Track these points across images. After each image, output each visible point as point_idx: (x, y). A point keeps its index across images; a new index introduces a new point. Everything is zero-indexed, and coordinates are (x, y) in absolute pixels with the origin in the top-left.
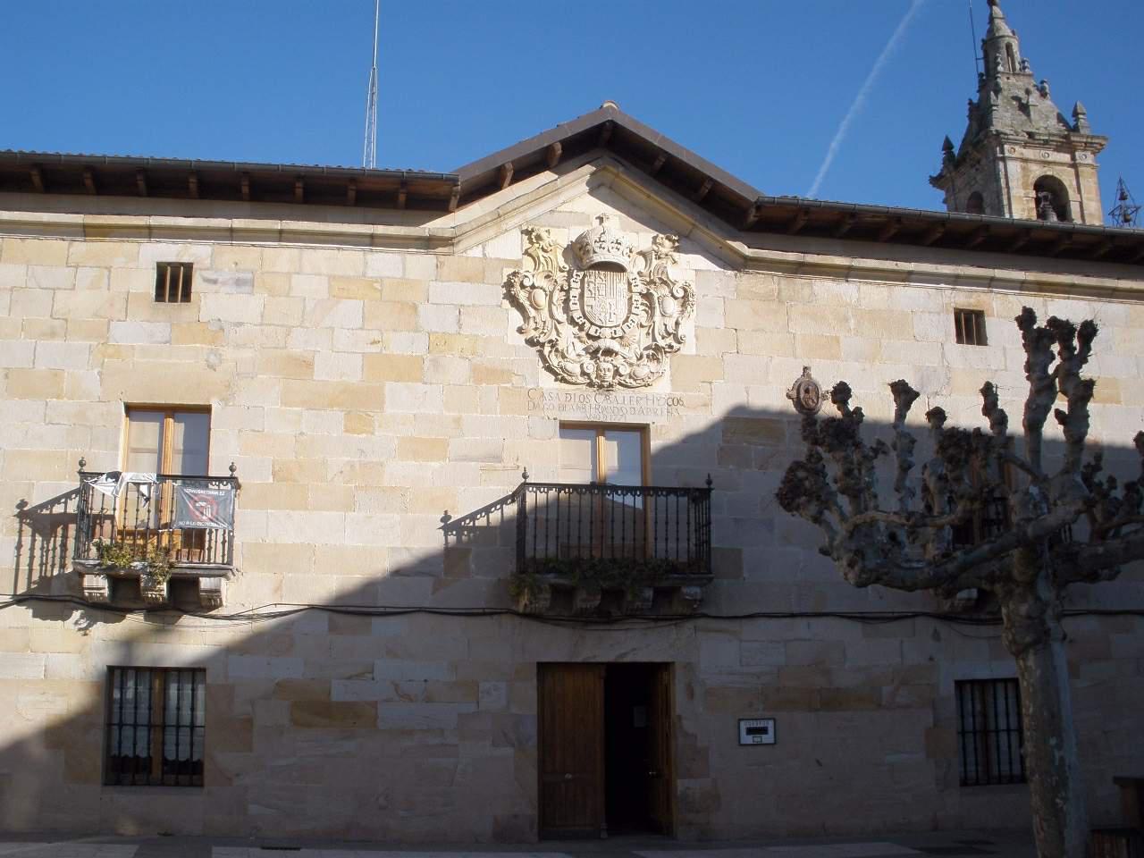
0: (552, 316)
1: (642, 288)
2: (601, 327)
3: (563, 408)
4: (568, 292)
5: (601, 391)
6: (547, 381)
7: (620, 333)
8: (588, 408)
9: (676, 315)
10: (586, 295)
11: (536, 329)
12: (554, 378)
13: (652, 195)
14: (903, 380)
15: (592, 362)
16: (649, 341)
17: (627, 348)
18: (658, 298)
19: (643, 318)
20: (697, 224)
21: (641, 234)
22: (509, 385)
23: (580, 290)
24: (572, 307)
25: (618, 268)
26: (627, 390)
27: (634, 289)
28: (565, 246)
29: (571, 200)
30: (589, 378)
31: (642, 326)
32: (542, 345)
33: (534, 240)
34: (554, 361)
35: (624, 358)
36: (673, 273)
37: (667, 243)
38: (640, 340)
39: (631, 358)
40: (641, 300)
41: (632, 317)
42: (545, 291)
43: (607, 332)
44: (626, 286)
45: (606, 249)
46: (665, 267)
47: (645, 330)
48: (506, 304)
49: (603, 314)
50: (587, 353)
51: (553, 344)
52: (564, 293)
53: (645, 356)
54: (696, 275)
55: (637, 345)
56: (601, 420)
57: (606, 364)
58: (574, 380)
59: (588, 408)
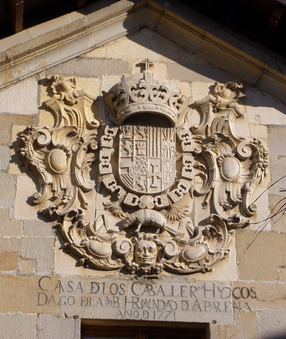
0: (75, 182)
1: (194, 146)
2: (140, 195)
3: (86, 302)
4: (97, 152)
5: (140, 279)
6: (66, 266)
7: (165, 202)
8: (121, 301)
9: (242, 180)
10: (120, 155)
11: (53, 199)
12: (75, 262)
13: (209, 35)
14: (80, 206)
15: (129, 240)
16: (206, 214)
17: (177, 223)
18: (218, 159)
19: (198, 185)
20: (266, 67)
21: (194, 84)
22: (13, 272)
23: (113, 150)
24: (102, 170)
25: (161, 121)
26: (176, 277)
27: (185, 148)
28: (95, 98)
29: (103, 44)
30: (124, 261)
31: (196, 194)
32: (61, 219)
33: (55, 91)
34: (76, 239)
35: (173, 235)
36: (236, 129)
37: (228, 93)
38: (195, 212)
39: (182, 235)
40: (194, 162)
41: (182, 182)
42: (66, 150)
43: (149, 201)
44: (174, 144)
45: (146, 97)
46: (227, 121)
47: (201, 200)
48: (14, 168)
49: (143, 178)
50: (121, 230)
51: (75, 217)
52: (92, 155)
53: (200, 233)
54: (269, 132)
55: (189, 219)
56: (141, 317)
57: (148, 242)
58: (102, 263)
59: (121, 301)
